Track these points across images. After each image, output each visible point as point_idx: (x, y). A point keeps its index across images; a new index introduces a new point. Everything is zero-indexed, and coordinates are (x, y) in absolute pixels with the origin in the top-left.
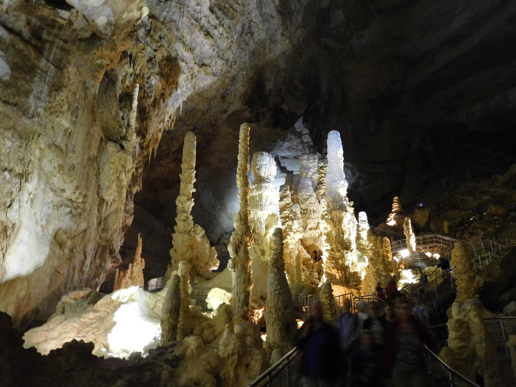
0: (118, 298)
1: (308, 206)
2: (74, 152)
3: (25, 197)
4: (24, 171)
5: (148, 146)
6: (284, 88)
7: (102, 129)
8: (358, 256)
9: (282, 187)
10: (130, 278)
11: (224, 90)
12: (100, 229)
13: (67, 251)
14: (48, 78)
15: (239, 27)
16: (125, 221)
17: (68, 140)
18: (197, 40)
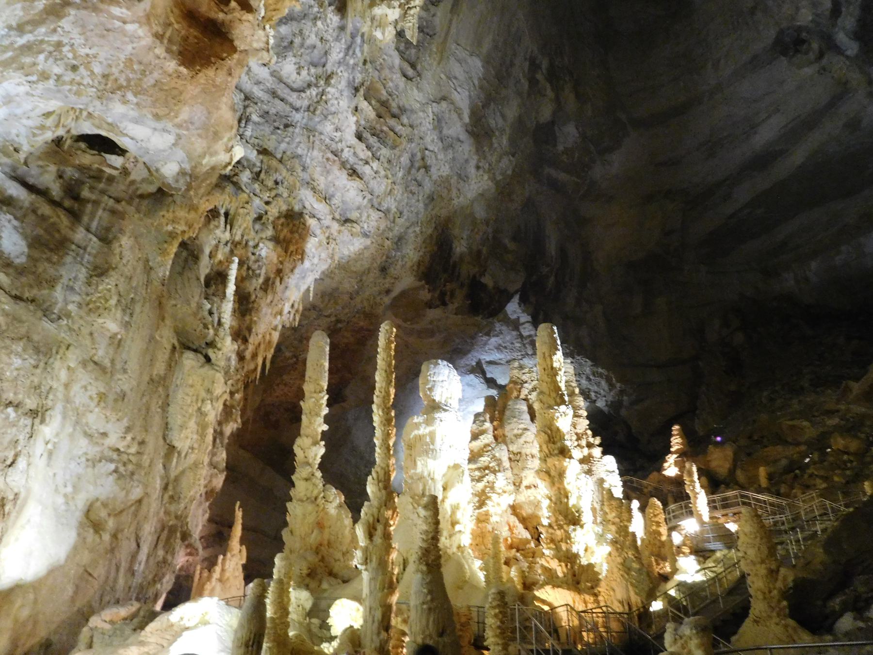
1: (522, 448)
2: (125, 371)
3: (39, 448)
4: (40, 405)
5: (254, 356)
6: (485, 250)
8: (597, 534)
9: (477, 416)
10: (220, 580)
11: (384, 257)
12: (166, 497)
13: (106, 537)
14: (87, 256)
15: (405, 160)
16: (210, 481)
17: (116, 353)
18: (337, 183)
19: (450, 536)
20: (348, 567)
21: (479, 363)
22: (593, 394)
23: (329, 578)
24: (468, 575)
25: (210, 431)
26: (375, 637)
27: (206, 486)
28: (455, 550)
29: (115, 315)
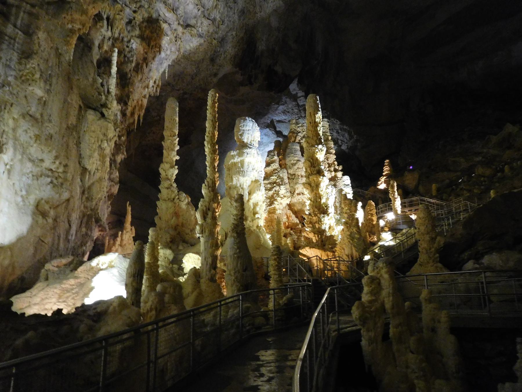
0: (98, 264)
1: (295, 171)
2: (50, 121)
5: (133, 114)
7: (80, 97)
8: (336, 219)
9: (269, 152)
10: (121, 245)
12: (84, 198)
13: (50, 221)
16: (110, 189)
19: (253, 221)
20: (194, 238)
21: (272, 121)
22: (340, 142)
23: (183, 244)
24: (262, 242)
25: (108, 159)
26: (208, 273)
27: (107, 192)
28: (255, 228)
29: (39, 84)
